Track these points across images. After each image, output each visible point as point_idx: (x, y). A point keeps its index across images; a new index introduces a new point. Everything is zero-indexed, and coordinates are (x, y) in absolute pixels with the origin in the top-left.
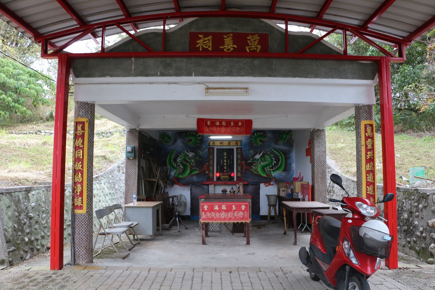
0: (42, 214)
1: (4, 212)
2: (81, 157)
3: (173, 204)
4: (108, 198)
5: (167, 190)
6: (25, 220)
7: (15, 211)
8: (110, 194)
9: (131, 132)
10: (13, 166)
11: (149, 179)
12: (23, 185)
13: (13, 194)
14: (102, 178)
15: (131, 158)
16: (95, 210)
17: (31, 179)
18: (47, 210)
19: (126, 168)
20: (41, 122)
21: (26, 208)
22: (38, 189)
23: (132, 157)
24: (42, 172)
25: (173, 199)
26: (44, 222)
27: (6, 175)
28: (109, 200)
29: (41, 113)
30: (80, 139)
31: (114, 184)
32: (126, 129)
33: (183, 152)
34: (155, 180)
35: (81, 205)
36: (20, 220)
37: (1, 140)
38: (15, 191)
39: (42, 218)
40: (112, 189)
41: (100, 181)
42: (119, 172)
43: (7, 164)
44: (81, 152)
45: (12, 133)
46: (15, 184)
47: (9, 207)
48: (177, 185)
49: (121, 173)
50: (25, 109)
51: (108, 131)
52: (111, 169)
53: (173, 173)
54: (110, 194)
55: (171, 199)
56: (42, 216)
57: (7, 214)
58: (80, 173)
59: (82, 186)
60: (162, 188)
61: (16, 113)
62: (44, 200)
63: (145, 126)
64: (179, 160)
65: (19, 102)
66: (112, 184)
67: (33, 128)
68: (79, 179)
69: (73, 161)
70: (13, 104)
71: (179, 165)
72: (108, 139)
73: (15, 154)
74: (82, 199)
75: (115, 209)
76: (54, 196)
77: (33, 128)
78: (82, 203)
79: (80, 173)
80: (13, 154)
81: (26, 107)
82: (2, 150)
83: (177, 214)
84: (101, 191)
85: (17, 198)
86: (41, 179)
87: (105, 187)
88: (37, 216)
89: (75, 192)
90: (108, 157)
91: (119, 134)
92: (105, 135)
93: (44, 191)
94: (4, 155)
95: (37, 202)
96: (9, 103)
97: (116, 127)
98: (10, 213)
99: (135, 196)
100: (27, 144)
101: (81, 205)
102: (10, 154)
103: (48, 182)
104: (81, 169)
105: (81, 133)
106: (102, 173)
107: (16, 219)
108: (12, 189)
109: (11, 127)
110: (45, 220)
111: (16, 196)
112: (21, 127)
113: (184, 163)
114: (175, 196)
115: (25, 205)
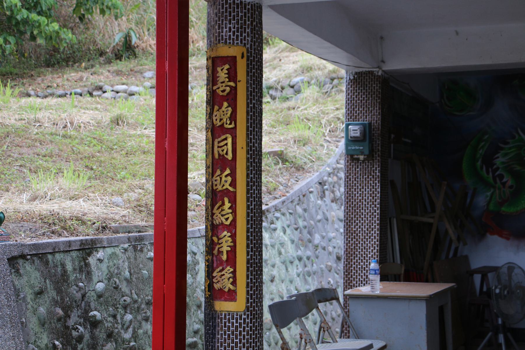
0: (123, 312)
1: (29, 306)
2: (230, 157)
3: (489, 294)
4: (293, 271)
5: (464, 251)
6: (81, 329)
7: (56, 303)
8: (300, 259)
9: (359, 82)
10: (42, 184)
11: (413, 218)
12: (72, 234)
13: (50, 257)
14: (278, 214)
15: (362, 157)
16: (267, 303)
17: (90, 217)
18: (136, 302)
19: (347, 186)
20: (100, 64)
21: (83, 296)
22: (111, 244)
23: (362, 153)
24: (117, 199)
25: (484, 278)
26: (127, 336)
27: (26, 207)
28: (298, 275)
29: (98, 39)
30: (225, 104)
31: (309, 233)
32: (343, 72)
33: (514, 137)
34: (431, 220)
35: (232, 287)
36: (67, 328)
37: (5, 113)
38: (55, 249)
39: (123, 325)
40: (306, 247)
41: (272, 223)
42: (322, 196)
43: (24, 178)
44: (230, 141)
45: (29, 95)
46: (53, 232)
47: (40, 293)
48: (496, 237)
49: (328, 199)
50: (55, 26)
51: (285, 83)
52: (300, 190)
53: (481, 201)
54: (300, 259)
55: (477, 278)
56: (122, 318)
57: (35, 311)
58: (226, 200)
59: (233, 236)
60: (451, 241)
61: (33, 38)
62: (127, 274)
63: (400, 61)
64: (500, 160)
65: (39, 9)
66: (305, 232)
67: (81, 79)
68: (224, 216)
69: (207, 167)
70: (25, 12)
71: (501, 177)
72: (286, 104)
73: (43, 152)
74: (234, 273)
75: (320, 302)
76: (159, 261)
77: (81, 79)
78: (234, 283)
79: (226, 200)
80: (38, 150)
81: (58, 22)
82: (8, 140)
83: (500, 321)
84: (275, 252)
85: (59, 269)
86: (117, 217)
87: (286, 238)
88: (110, 319)
89: (215, 252)
90: (291, 155)
91: (317, 89)
92: (278, 94)
93: (126, 250)
94: (16, 155)
95: (109, 279)
96: (12, 11)
97: (309, 69)
98: (42, 310)
99: (374, 265)
100: (72, 123)
101: (232, 287)
102: (31, 152)
103: (136, 227)
104: (231, 189)
105: (228, 89)
106: (276, 202)
107: (59, 326)
108: (48, 245)
109: (23, 78)
110: (131, 330)
111: (55, 263)
112: (49, 77)
113: (518, 168)
114: (495, 269)
115: (80, 288)
